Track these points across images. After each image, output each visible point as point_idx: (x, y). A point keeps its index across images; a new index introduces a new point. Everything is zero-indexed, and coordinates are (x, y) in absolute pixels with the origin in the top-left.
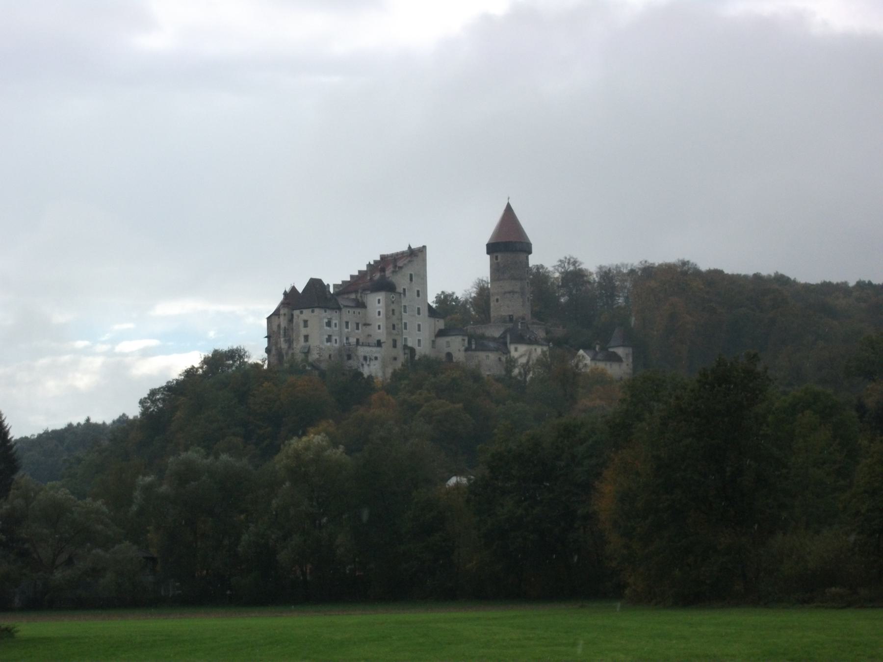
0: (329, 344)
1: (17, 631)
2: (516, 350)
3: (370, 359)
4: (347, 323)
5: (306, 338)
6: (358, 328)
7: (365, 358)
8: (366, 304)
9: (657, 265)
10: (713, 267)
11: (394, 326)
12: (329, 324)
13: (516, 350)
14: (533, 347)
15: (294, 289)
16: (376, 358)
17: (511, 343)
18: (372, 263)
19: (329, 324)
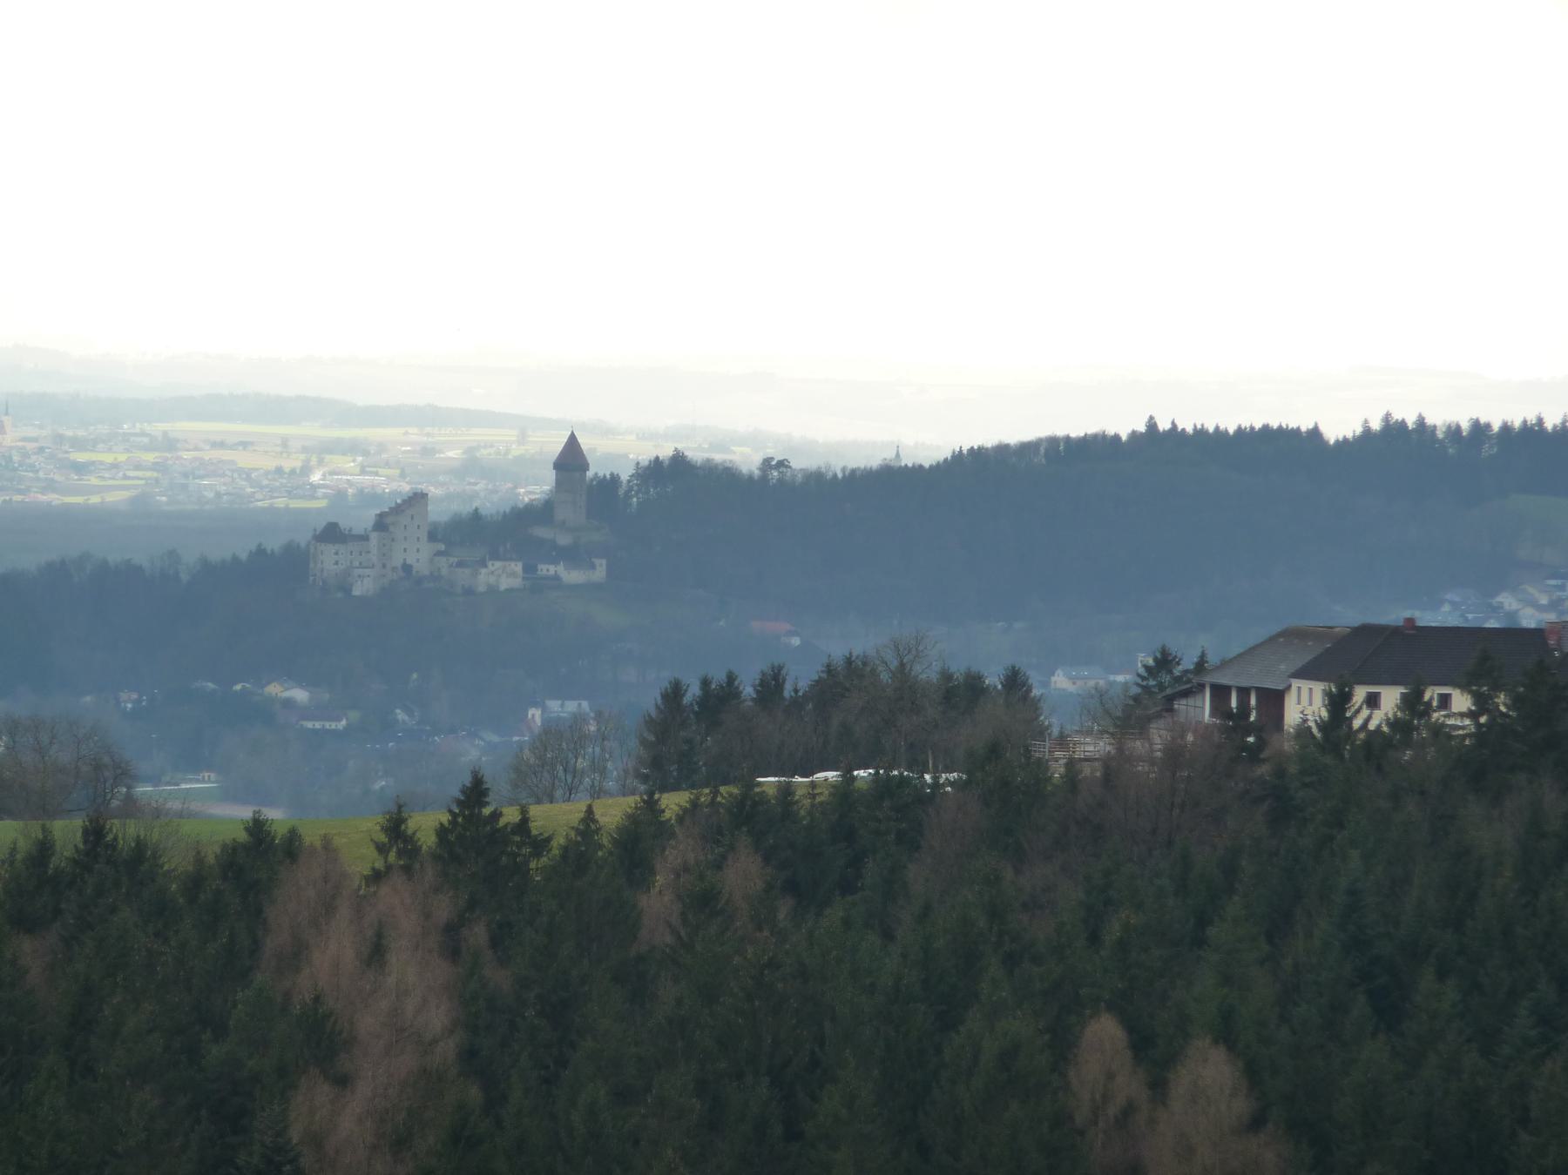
0: (336, 567)
1: (961, 451)
2: (493, 565)
3: (363, 577)
4: (352, 552)
5: (322, 563)
6: (361, 555)
7: (359, 576)
8: (274, 544)
9: (244, 556)
10: (1092, 428)
11: (384, 555)
12: (336, 553)
13: (493, 565)
14: (507, 563)
15: (972, 448)
16: (369, 576)
17: (490, 559)
18: (976, 448)
19: (336, 553)
